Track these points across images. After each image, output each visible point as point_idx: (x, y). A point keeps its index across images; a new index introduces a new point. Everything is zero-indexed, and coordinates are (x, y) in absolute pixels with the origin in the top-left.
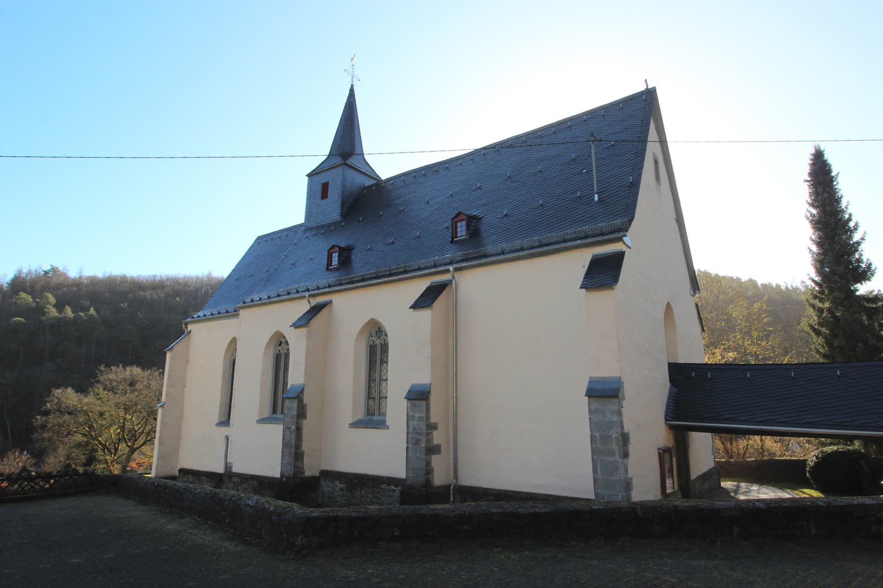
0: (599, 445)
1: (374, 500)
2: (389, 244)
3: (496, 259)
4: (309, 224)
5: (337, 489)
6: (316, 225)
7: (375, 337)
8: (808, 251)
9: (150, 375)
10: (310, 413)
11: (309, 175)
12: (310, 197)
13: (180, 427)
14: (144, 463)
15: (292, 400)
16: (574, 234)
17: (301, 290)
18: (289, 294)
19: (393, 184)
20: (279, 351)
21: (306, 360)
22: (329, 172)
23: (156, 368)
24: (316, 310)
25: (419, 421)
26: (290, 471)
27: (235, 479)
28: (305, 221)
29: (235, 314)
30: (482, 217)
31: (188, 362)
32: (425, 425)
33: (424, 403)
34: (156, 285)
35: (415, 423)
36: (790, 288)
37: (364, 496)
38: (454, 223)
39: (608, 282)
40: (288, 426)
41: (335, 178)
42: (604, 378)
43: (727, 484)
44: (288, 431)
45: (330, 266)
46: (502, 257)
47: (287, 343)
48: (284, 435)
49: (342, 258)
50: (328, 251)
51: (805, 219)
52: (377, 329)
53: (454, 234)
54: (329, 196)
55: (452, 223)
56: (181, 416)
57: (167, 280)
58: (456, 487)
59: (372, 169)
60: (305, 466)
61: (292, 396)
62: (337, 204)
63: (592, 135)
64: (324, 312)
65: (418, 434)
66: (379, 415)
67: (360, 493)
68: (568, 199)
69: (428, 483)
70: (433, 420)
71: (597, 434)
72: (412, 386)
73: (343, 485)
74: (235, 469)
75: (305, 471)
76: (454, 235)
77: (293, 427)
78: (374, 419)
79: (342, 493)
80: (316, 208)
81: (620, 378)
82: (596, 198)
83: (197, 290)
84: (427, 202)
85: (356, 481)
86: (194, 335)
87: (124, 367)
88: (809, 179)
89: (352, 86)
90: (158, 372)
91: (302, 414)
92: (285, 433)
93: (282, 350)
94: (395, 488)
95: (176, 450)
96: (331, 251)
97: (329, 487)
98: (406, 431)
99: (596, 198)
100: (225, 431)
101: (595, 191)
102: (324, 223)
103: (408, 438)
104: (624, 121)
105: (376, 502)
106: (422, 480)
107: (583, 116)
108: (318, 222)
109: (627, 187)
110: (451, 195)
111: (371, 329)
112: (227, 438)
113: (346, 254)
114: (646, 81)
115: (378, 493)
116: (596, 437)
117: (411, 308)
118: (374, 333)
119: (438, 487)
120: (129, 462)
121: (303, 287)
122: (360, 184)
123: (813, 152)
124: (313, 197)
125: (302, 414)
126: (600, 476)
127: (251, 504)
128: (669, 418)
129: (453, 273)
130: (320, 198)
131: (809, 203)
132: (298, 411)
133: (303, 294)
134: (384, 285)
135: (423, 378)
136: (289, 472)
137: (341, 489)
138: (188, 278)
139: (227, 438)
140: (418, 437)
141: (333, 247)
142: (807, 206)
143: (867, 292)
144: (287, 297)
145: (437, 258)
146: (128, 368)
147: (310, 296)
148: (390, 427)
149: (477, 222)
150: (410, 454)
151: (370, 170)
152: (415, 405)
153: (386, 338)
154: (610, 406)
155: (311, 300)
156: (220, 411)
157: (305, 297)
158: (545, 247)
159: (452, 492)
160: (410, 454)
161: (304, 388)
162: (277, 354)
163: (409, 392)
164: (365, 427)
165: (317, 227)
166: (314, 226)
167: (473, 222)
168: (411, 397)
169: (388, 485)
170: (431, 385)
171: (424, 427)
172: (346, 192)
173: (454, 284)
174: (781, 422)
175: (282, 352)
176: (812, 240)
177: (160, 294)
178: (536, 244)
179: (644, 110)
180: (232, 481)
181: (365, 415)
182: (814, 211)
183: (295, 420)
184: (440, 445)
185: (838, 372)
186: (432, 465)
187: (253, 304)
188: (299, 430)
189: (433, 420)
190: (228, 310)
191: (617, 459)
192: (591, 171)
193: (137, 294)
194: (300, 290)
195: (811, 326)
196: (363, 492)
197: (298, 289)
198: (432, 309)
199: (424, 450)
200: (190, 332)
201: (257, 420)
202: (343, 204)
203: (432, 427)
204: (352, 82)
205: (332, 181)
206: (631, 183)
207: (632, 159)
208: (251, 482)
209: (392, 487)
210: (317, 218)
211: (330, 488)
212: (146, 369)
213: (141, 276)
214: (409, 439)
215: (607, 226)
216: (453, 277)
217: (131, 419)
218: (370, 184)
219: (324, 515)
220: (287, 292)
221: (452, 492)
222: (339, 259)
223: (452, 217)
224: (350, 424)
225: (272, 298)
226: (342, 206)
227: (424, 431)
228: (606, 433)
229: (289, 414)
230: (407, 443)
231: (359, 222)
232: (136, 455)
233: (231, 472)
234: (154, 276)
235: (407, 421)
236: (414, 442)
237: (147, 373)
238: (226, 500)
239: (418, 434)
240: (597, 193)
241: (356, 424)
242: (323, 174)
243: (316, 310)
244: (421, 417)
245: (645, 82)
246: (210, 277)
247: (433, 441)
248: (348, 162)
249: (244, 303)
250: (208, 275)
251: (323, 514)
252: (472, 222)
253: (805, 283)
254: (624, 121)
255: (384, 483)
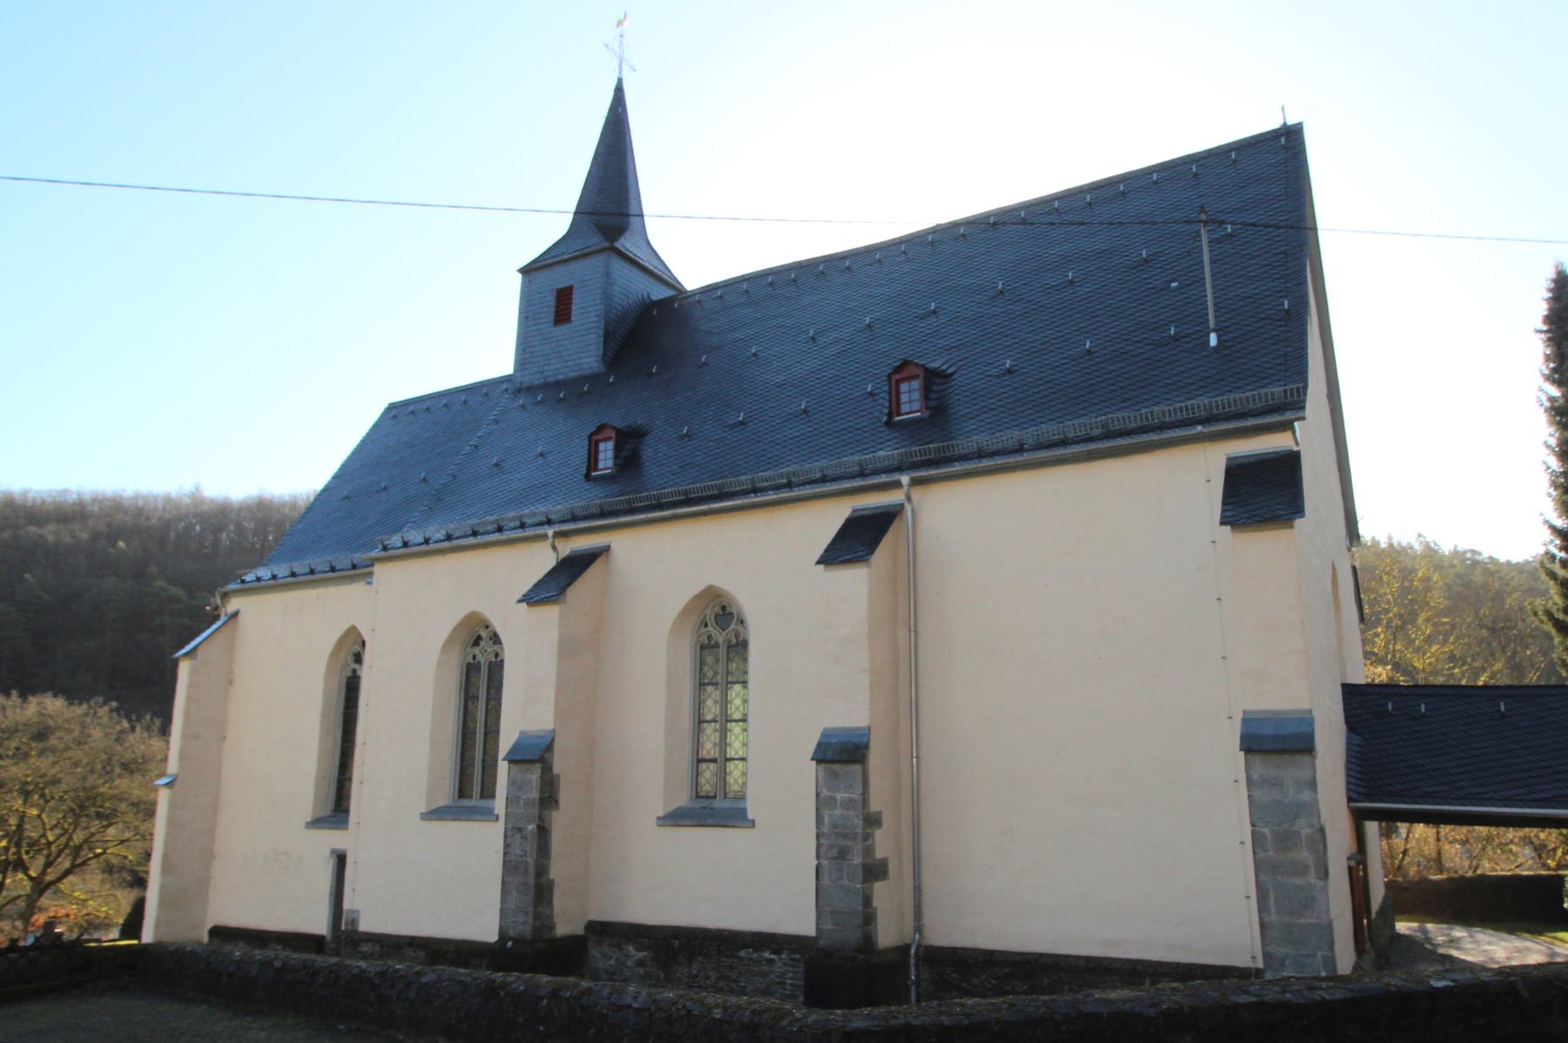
0: (1271, 853)
1: (722, 984)
2: (734, 426)
3: (992, 463)
4: (526, 379)
5: (629, 963)
6: (542, 381)
7: (714, 628)
8: (1544, 467)
9: (86, 715)
10: (565, 794)
11: (526, 271)
12: (527, 318)
13: (211, 832)
14: (67, 915)
15: (525, 766)
16: (1179, 414)
17: (529, 521)
18: (500, 529)
19: (721, 297)
20: (474, 657)
21: (559, 676)
22: (574, 266)
23: (101, 700)
24: (571, 569)
25: (846, 809)
26: (523, 926)
27: (365, 948)
28: (515, 370)
29: (359, 571)
30: (952, 374)
31: (231, 683)
32: (861, 816)
33: (857, 768)
34: (69, 513)
35: (838, 812)
36: (1396, 545)
37: (696, 976)
38: (893, 383)
39: (1283, 512)
40: (516, 826)
41: (582, 276)
42: (1276, 712)
43: (1403, 927)
44: (518, 836)
45: (595, 471)
46: (1018, 458)
47: (496, 639)
48: (507, 846)
49: (623, 454)
50: (590, 437)
51: (1537, 405)
52: (718, 610)
53: (895, 407)
54: (573, 319)
55: (890, 384)
56: (214, 808)
57: (95, 500)
58: (922, 948)
59: (662, 261)
60: (555, 912)
61: (528, 757)
62: (593, 336)
63: (1202, 210)
64: (595, 570)
65: (845, 836)
66: (725, 797)
67: (686, 970)
68: (1147, 341)
69: (868, 943)
70: (874, 806)
71: (1266, 831)
72: (826, 734)
73: (645, 953)
74: (365, 926)
75: (555, 925)
76: (894, 408)
77: (532, 827)
78: (714, 806)
79: (642, 972)
80: (542, 342)
81: (1310, 712)
82: (1213, 340)
83: (167, 525)
84: (813, 339)
85: (676, 944)
86: (245, 620)
87: (24, 696)
88: (1545, 328)
89: (620, 81)
90: (106, 708)
91: (550, 797)
92: (509, 840)
93: (482, 654)
94: (772, 956)
95: (202, 887)
96: (595, 438)
97: (610, 959)
98: (814, 830)
99: (1213, 340)
100: (333, 839)
101: (1212, 323)
102: (561, 377)
103: (819, 846)
104: (1243, 187)
105: (726, 988)
106: (853, 936)
107: (1151, 173)
108: (545, 374)
109: (1280, 320)
110: (869, 326)
111: (704, 610)
112: (341, 860)
113: (630, 443)
114: (1283, 108)
115: (731, 968)
116: (1264, 836)
117: (819, 562)
118: (710, 619)
119: (887, 951)
120: (33, 914)
121: (492, 522)
122: (642, 295)
123: (1552, 274)
124: (535, 319)
125: (550, 797)
126: (1273, 917)
127: (636, 1005)
128: (1355, 796)
129: (909, 490)
130: (552, 323)
131: (1543, 375)
132: (542, 791)
133: (540, 531)
134: (740, 513)
135: (851, 714)
136: (522, 928)
137: (641, 963)
138: (145, 498)
139: (341, 860)
140: (844, 843)
141: (601, 429)
142: (1541, 379)
143: (1535, 557)
144: (497, 536)
145: (824, 463)
146: (33, 700)
147: (557, 535)
148: (756, 823)
149: (943, 384)
150: (826, 881)
151: (660, 267)
152: (836, 775)
153: (740, 629)
154: (1290, 771)
155: (560, 544)
156: (316, 794)
157: (545, 537)
158: (1119, 439)
159: (912, 961)
160: (826, 881)
161: (553, 740)
162: (469, 664)
163: (820, 745)
164: (699, 824)
165: (546, 386)
166: (536, 382)
167: (934, 380)
168: (829, 756)
169: (756, 951)
170: (869, 730)
171: (859, 822)
172: (614, 311)
173: (909, 514)
174: (1540, 800)
175: (482, 660)
176: (1548, 446)
177: (78, 533)
178: (1096, 432)
179: (1287, 166)
180: (360, 952)
181: (691, 799)
182: (1555, 392)
183: (536, 811)
184: (887, 859)
185: (1390, 706)
186: (875, 904)
187: (408, 551)
188: (543, 832)
189: (874, 806)
190: (334, 564)
191: (1313, 881)
192: (1216, 280)
193: (22, 533)
194: (529, 521)
195: (1548, 613)
196: (695, 968)
197: (524, 520)
198: (869, 566)
199: (860, 871)
200: (235, 615)
201: (422, 814)
202: (607, 335)
203: (873, 821)
204: (620, 72)
205: (582, 284)
206: (1287, 312)
207: (1279, 263)
208: (410, 952)
209: (767, 955)
210: (544, 365)
211: (612, 962)
212: (76, 701)
213: (30, 490)
214: (823, 850)
215: (1251, 399)
216: (909, 499)
217: (39, 816)
218: (661, 297)
219: (878, 1026)
220: (496, 526)
221: (912, 961)
222: (616, 456)
223: (890, 371)
224: (658, 818)
225: (458, 538)
226: (605, 342)
227: (859, 830)
228: (1286, 826)
229: (519, 797)
230: (818, 857)
231: (651, 375)
232: (44, 901)
233: (357, 932)
234: (65, 491)
235: (817, 809)
236: (836, 855)
237: (80, 710)
238: (542, 998)
239: (845, 836)
240: (1215, 330)
241: (675, 818)
242: (557, 269)
243: (571, 569)
244: (851, 800)
245: (1281, 111)
246: (197, 499)
247: (874, 851)
248: (617, 245)
249: (385, 548)
250: (193, 493)
251: (876, 1022)
252: (934, 384)
253: (1424, 537)
254: (1243, 187)
255: (746, 947)
